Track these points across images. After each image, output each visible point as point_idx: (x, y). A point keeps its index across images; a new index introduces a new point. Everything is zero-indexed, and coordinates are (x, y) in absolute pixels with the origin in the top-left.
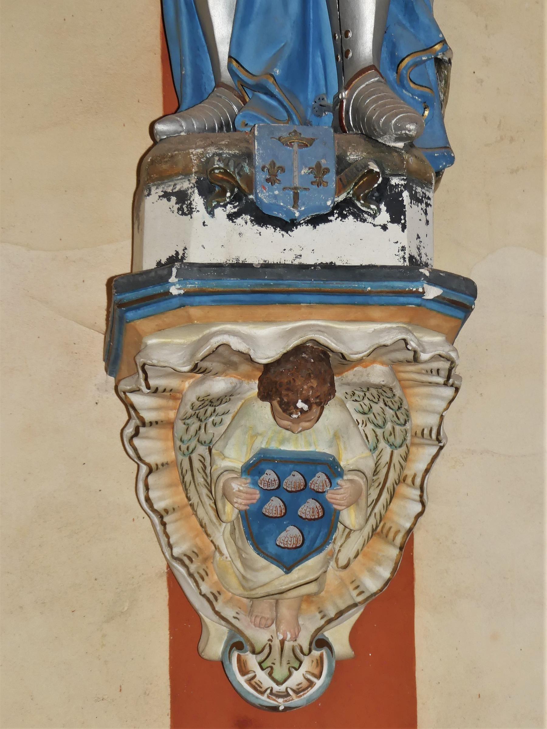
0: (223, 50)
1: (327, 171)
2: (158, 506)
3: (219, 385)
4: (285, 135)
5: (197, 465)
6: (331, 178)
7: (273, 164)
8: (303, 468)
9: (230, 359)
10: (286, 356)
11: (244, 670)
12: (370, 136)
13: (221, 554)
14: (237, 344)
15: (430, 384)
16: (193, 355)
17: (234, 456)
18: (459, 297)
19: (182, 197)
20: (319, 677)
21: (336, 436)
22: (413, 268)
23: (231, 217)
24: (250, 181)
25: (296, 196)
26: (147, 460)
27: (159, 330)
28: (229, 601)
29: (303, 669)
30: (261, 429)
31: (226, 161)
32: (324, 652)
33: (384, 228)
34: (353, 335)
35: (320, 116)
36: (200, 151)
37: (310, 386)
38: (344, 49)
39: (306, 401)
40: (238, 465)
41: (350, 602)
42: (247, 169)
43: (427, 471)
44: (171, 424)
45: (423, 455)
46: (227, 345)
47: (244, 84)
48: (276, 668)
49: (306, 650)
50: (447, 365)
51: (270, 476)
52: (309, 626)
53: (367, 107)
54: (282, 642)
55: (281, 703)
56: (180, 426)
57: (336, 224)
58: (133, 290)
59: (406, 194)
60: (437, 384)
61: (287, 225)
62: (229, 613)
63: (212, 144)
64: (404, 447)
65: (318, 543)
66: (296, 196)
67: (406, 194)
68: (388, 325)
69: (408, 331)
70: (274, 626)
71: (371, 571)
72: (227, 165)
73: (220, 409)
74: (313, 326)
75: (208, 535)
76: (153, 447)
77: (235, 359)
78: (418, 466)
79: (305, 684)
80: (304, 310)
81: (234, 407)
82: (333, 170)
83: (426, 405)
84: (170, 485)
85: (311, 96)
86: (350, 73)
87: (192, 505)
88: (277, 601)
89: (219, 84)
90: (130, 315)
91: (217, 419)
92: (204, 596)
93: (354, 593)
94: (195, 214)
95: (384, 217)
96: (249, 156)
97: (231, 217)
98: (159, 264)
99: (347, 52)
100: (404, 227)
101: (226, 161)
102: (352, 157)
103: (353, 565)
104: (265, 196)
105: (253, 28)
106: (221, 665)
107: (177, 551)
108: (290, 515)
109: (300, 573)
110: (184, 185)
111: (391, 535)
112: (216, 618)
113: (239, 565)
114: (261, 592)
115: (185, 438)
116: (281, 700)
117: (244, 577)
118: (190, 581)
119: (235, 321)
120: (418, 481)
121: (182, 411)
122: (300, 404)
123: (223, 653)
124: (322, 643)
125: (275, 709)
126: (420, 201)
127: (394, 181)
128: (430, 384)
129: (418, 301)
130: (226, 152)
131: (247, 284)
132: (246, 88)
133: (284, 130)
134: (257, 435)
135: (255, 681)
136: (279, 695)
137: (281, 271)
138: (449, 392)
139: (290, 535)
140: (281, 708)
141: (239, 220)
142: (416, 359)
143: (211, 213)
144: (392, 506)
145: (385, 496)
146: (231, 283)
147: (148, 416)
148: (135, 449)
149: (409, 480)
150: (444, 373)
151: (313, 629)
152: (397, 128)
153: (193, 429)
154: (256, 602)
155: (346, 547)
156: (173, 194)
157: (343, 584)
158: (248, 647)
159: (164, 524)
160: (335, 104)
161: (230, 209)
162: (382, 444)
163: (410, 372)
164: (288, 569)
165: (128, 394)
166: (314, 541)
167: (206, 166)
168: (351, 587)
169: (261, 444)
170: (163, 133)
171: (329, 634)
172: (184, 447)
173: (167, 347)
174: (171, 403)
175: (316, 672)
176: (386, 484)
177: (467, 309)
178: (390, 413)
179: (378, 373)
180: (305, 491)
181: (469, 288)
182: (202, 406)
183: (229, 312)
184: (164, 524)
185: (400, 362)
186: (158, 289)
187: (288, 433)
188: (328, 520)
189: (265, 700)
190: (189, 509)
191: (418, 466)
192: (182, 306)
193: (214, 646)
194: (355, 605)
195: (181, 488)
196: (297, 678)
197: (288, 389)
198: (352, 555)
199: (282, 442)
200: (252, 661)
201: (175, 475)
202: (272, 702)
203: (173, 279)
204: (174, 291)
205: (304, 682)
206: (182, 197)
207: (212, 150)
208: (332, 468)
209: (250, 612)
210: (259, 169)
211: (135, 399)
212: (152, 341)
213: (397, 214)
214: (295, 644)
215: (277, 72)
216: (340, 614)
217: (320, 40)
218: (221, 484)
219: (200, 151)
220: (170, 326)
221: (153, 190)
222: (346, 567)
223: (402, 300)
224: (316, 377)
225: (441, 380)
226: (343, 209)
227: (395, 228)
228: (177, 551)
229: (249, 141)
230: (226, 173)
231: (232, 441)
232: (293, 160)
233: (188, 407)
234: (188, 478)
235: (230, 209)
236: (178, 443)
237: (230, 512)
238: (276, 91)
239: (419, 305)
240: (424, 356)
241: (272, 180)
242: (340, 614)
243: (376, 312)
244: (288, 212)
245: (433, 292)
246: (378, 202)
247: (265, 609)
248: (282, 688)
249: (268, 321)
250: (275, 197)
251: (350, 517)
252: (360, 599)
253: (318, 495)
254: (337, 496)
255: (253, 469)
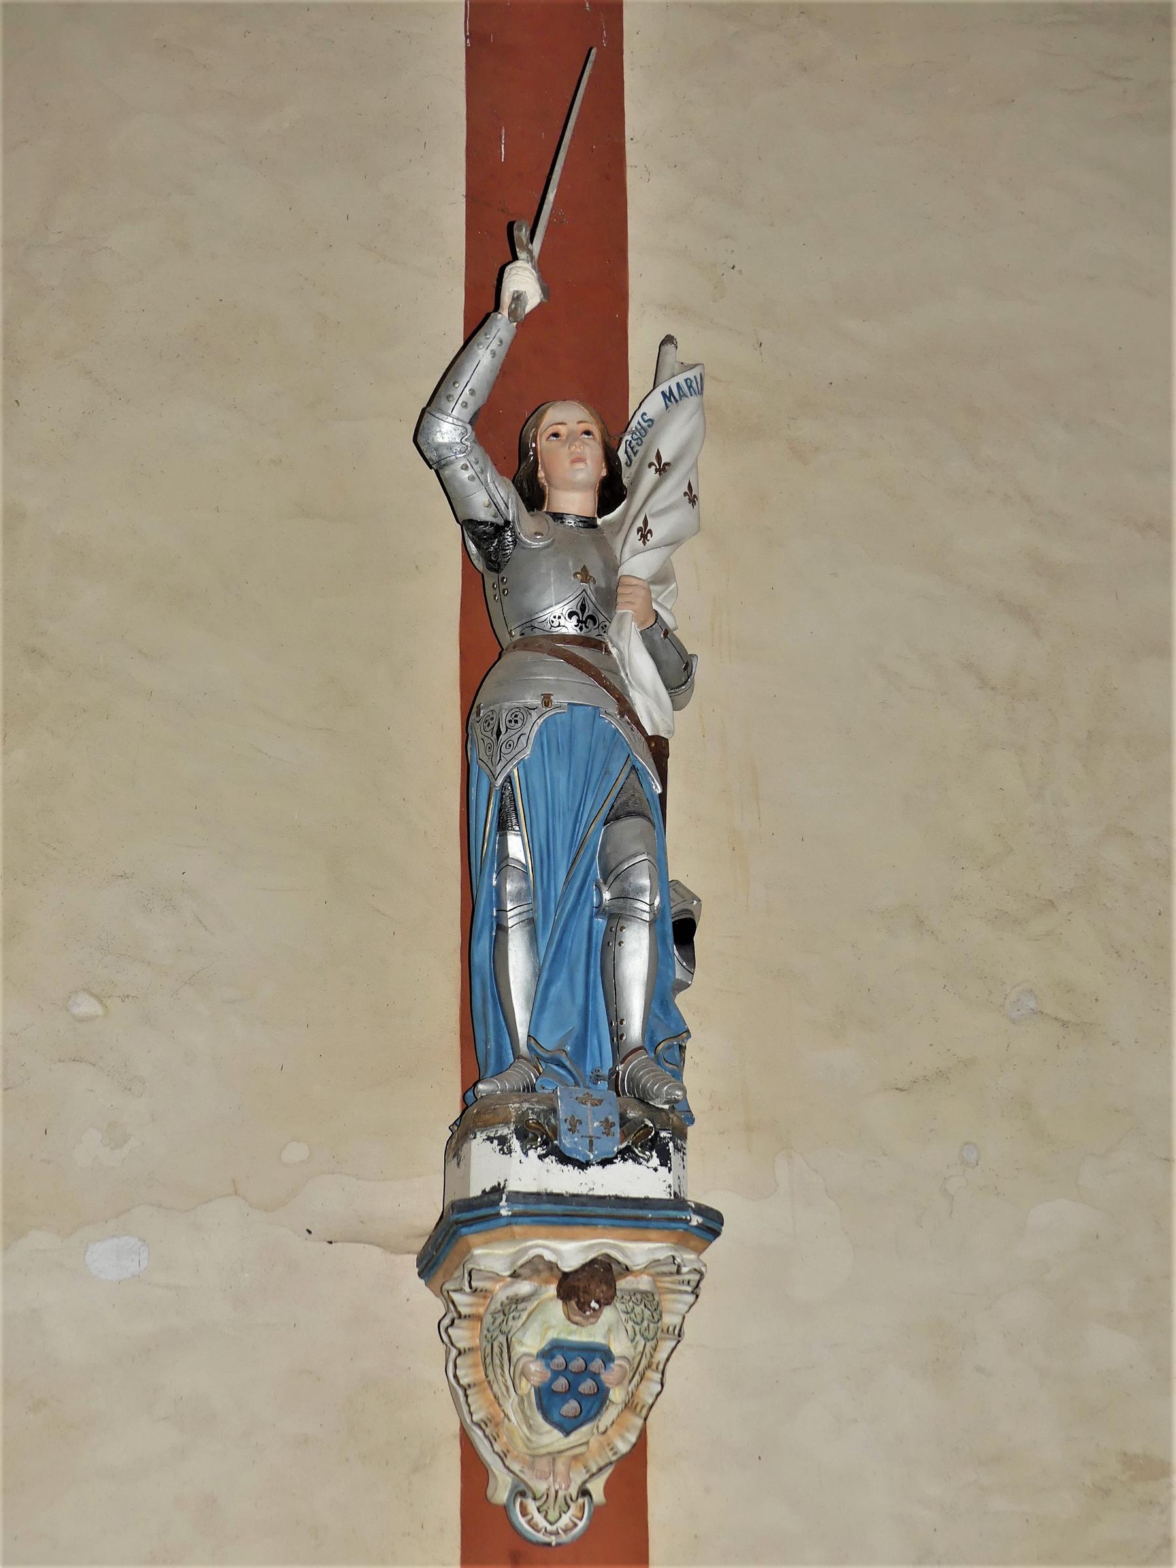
0: (522, 1032)
1: (613, 1124)
2: (464, 1381)
3: (524, 1287)
4: (580, 1095)
5: (496, 1350)
6: (617, 1130)
7: (573, 1117)
8: (585, 1355)
9: (538, 1268)
10: (583, 1267)
11: (524, 1513)
12: (643, 1101)
13: (509, 1420)
14: (549, 1256)
15: (680, 1292)
16: (513, 1263)
17: (530, 1343)
18: (712, 1225)
19: (503, 1141)
20: (581, 1519)
21: (609, 1330)
22: (678, 1202)
23: (541, 1157)
24: (555, 1131)
25: (591, 1143)
26: (458, 1345)
27: (486, 1243)
28: (516, 1458)
29: (570, 1513)
30: (554, 1322)
31: (538, 1114)
32: (586, 1500)
33: (656, 1170)
34: (639, 1252)
35: (596, 1084)
36: (517, 1105)
37: (601, 1291)
38: (617, 1035)
39: (597, 1302)
40: (535, 1352)
41: (607, 1461)
42: (553, 1121)
43: (668, 1359)
44: (479, 1318)
45: (666, 1346)
46: (541, 1257)
47: (539, 1058)
48: (551, 1512)
49: (574, 1497)
50: (697, 1277)
51: (559, 1360)
52: (578, 1478)
53: (641, 1077)
54: (557, 1492)
55: (553, 1540)
56: (488, 1319)
57: (619, 1165)
58: (468, 1211)
59: (671, 1144)
60: (686, 1292)
61: (583, 1165)
62: (516, 1467)
63: (526, 1101)
64: (655, 1340)
65: (592, 1412)
66: (591, 1143)
67: (671, 1144)
68: (660, 1245)
69: (676, 1250)
70: (551, 1479)
71: (622, 1437)
72: (539, 1116)
73: (520, 1306)
74: (603, 1244)
75: (500, 1405)
76: (463, 1335)
77: (541, 1267)
78: (661, 1356)
79: (571, 1524)
80: (599, 1230)
81: (531, 1306)
82: (618, 1125)
83: (673, 1309)
84: (475, 1365)
85: (589, 1068)
86: (624, 1053)
87: (489, 1382)
88: (554, 1459)
89: (517, 1056)
90: (464, 1230)
91: (515, 1314)
92: (497, 1454)
93: (610, 1454)
94: (513, 1154)
95: (655, 1161)
96: (554, 1111)
97: (541, 1157)
98: (484, 1191)
99: (622, 1035)
100: (670, 1170)
101: (538, 1114)
102: (631, 1114)
103: (609, 1432)
104: (567, 1142)
105: (547, 1015)
106: (505, 1509)
107: (475, 1418)
108: (572, 1391)
109: (575, 1437)
110: (504, 1131)
111: (639, 1408)
112: (505, 1471)
113: (525, 1430)
114: (543, 1451)
115: (492, 1328)
116: (553, 1538)
117: (528, 1439)
118: (486, 1442)
119: (547, 1238)
120: (661, 1367)
121: (492, 1307)
122: (594, 1304)
123: (508, 1499)
124: (584, 1492)
125: (549, 1544)
126: (679, 1150)
127: (663, 1134)
128: (680, 1292)
129: (685, 1226)
130: (537, 1107)
131: (559, 1209)
132: (537, 1058)
133: (580, 1092)
134: (549, 1328)
135: (535, 1523)
136: (551, 1533)
137: (584, 1200)
138: (691, 1298)
139: (571, 1407)
140: (554, 1544)
141: (547, 1160)
142: (678, 1272)
143: (526, 1154)
144: (641, 1387)
145: (637, 1377)
146: (547, 1208)
147: (464, 1311)
148: (449, 1337)
149: (654, 1367)
150: (693, 1284)
151: (579, 1482)
152: (667, 1093)
153: (498, 1321)
154: (537, 1460)
155: (609, 1416)
156: (495, 1138)
157: (601, 1447)
158: (529, 1494)
159: (466, 1396)
160: (611, 1075)
161: (540, 1151)
162: (638, 1337)
163: (666, 1283)
164: (567, 1433)
165: (451, 1294)
166: (589, 1411)
167: (522, 1118)
168: (608, 1449)
169: (552, 1335)
170: (484, 1091)
171: (589, 1486)
172: (489, 1336)
173: (492, 1255)
174: (481, 1301)
175: (580, 1515)
176: (638, 1371)
177: (716, 1234)
178: (647, 1313)
179: (644, 1283)
180: (586, 1372)
181: (718, 1218)
182: (510, 1304)
183: (543, 1230)
184: (466, 1396)
185: (664, 1274)
186: (491, 1211)
187: (575, 1327)
188: (601, 1397)
189: (541, 1537)
190: (486, 1384)
191: (661, 1356)
192: (509, 1224)
193: (500, 1493)
194: (611, 1463)
195: (482, 1368)
196: (565, 1520)
197: (584, 1292)
198: (609, 1423)
199: (570, 1333)
200: (532, 1506)
201: (478, 1357)
202: (546, 1539)
203: (503, 1203)
204: (504, 1212)
205: (569, 1523)
206: (503, 1141)
207: (526, 1106)
208: (607, 1356)
209: (532, 1467)
210: (562, 1122)
211: (456, 1297)
212: (477, 1252)
213: (665, 1160)
214: (567, 1493)
215: (568, 1048)
216: (600, 1470)
217: (597, 1026)
218: (520, 1365)
219: (517, 1105)
220: (498, 1240)
221: (478, 1134)
222: (604, 1433)
223: (673, 1225)
224: (606, 1283)
225: (689, 1289)
226: (625, 1154)
227: (663, 1170)
228: (475, 1418)
229: (552, 1097)
230: (538, 1123)
231: (529, 1333)
232: (588, 1115)
233: (499, 1304)
234: (488, 1360)
235: (540, 1151)
236: (485, 1332)
237: (526, 1387)
238: (567, 1063)
239: (686, 1230)
240: (684, 1270)
241: (572, 1130)
242: (600, 1470)
243: (653, 1234)
244: (585, 1155)
245: (696, 1220)
246: (651, 1150)
247: (543, 1465)
248: (554, 1528)
249: (572, 1238)
250: (575, 1143)
251: (617, 1395)
252: (614, 1458)
253: (595, 1376)
254: (607, 1377)
255: (547, 1354)
